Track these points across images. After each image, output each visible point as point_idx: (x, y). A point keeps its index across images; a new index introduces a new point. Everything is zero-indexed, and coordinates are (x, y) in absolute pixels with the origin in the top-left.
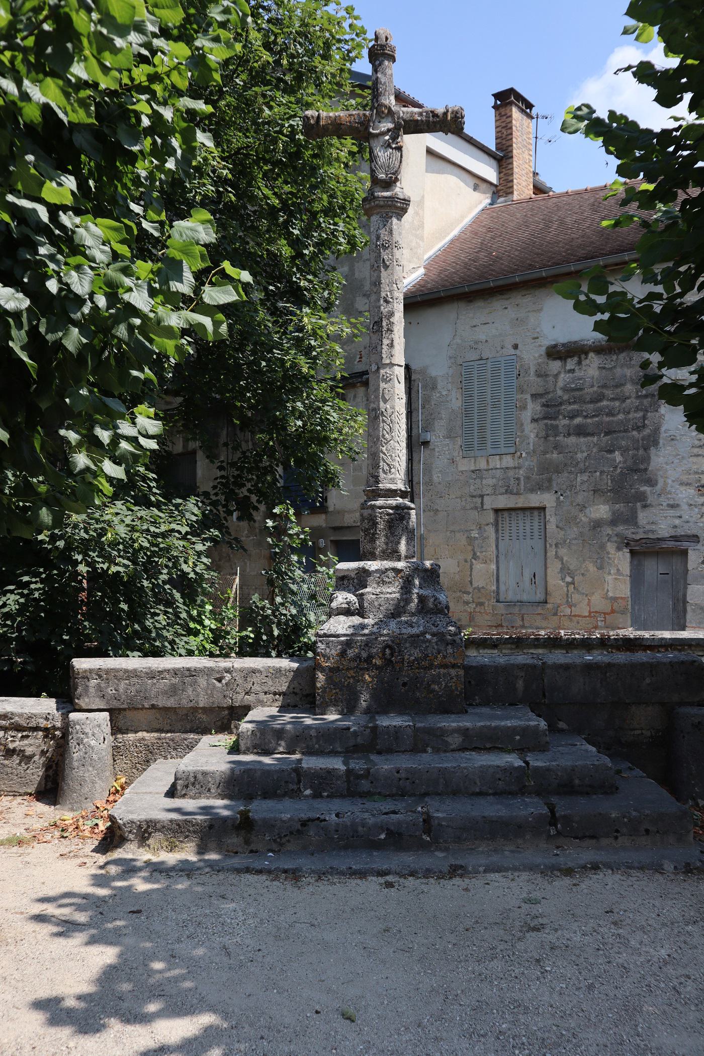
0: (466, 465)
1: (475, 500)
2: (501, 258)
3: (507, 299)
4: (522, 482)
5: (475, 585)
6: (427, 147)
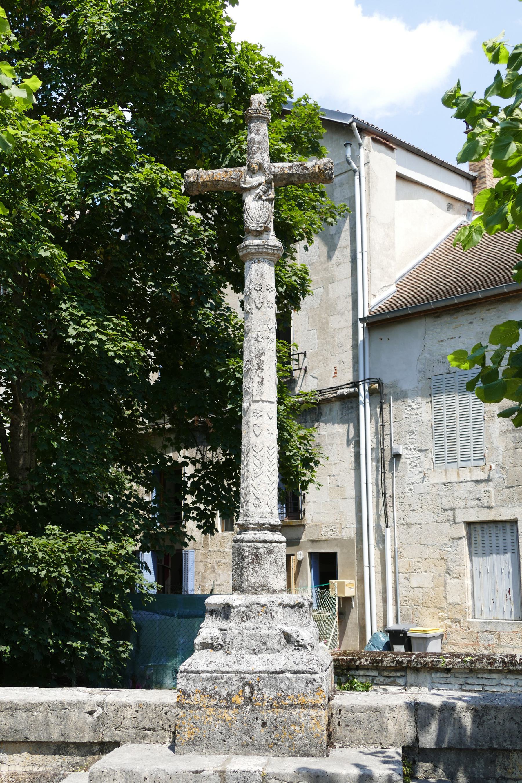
0: (437, 477)
1: (446, 513)
2: (469, 274)
3: (472, 314)
4: (493, 496)
5: (450, 600)
6: (397, 172)
